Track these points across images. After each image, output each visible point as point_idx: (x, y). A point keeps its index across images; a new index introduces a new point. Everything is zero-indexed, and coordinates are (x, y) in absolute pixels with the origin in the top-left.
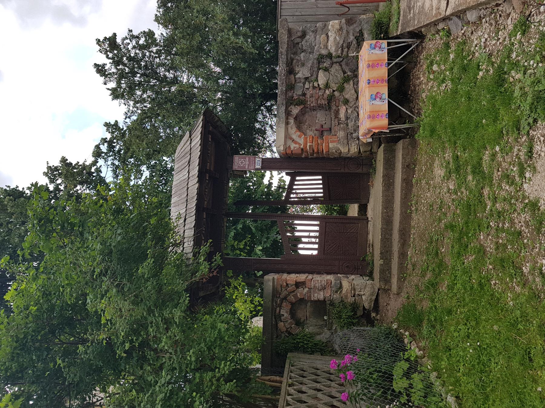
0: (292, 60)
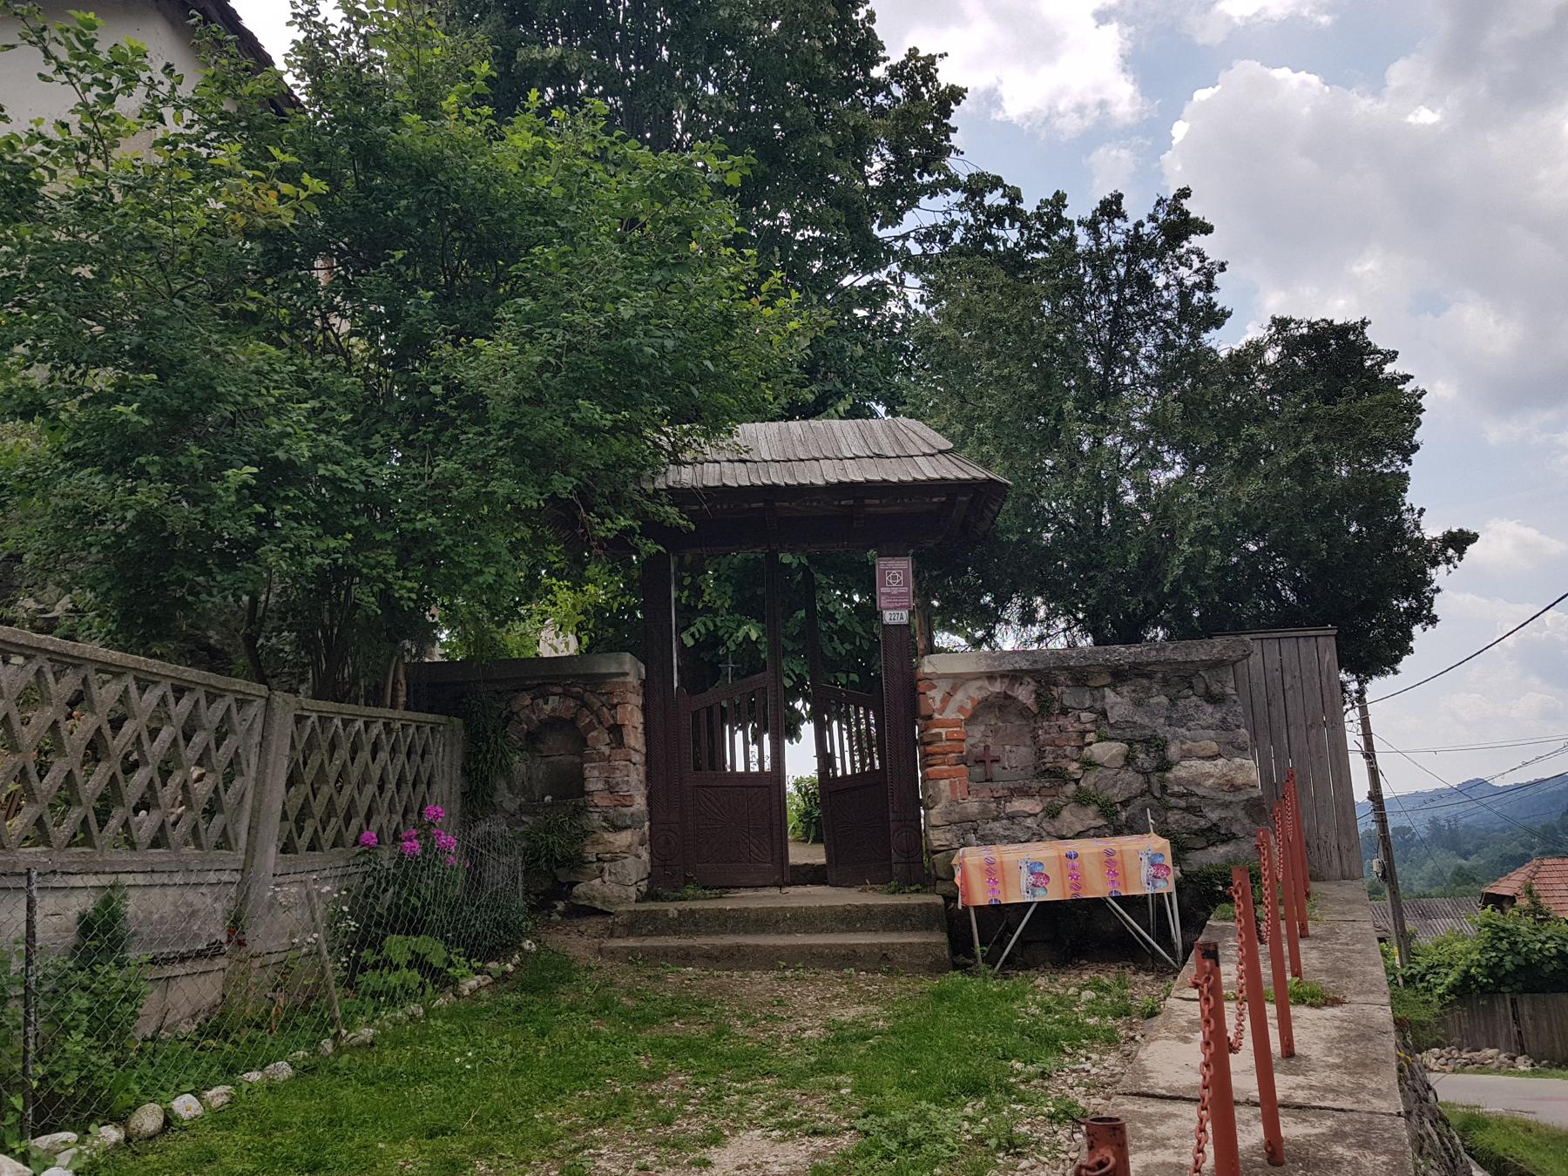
0: (1149, 676)
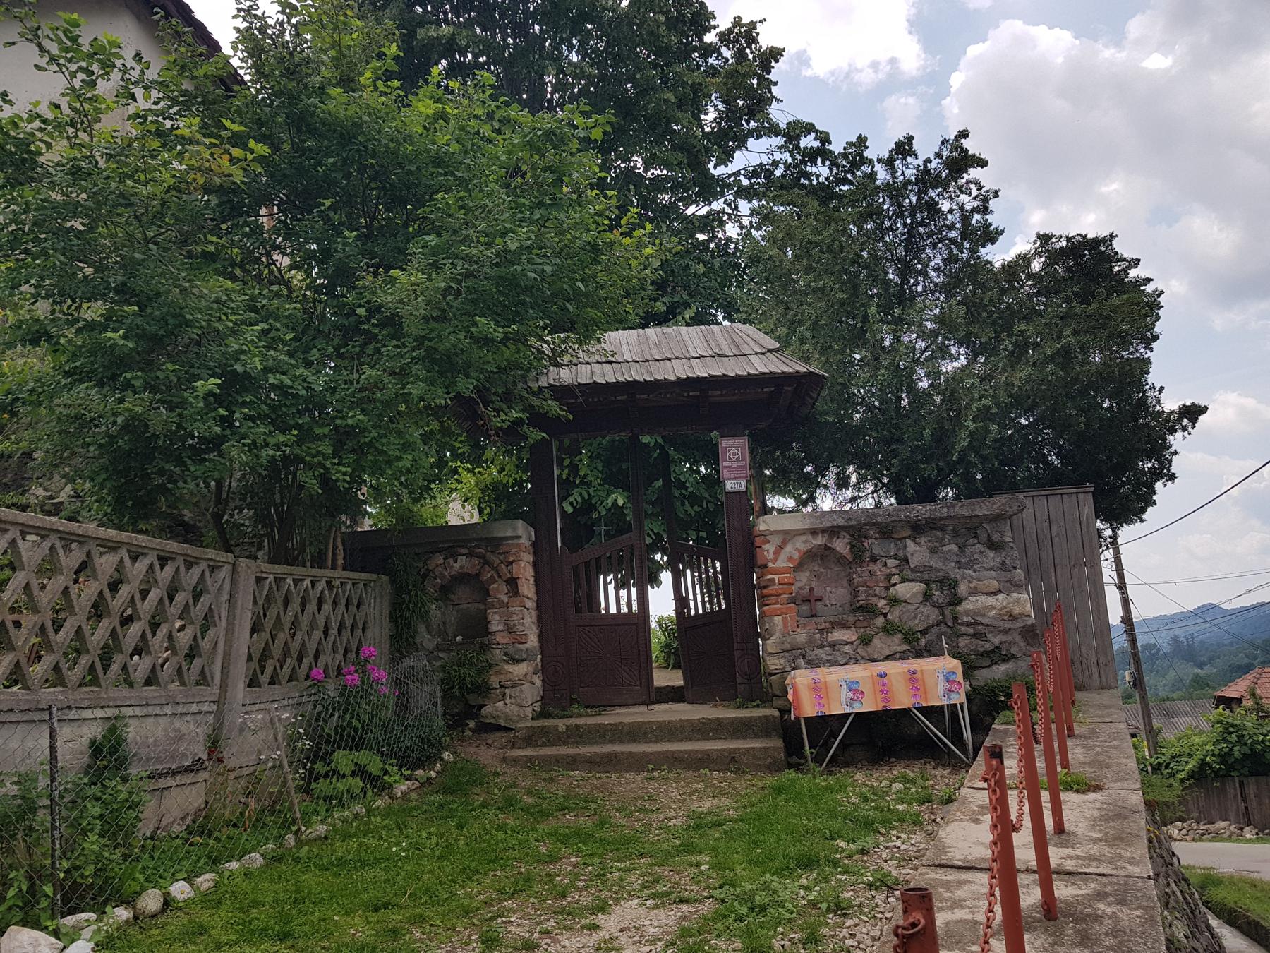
0: (942, 529)
